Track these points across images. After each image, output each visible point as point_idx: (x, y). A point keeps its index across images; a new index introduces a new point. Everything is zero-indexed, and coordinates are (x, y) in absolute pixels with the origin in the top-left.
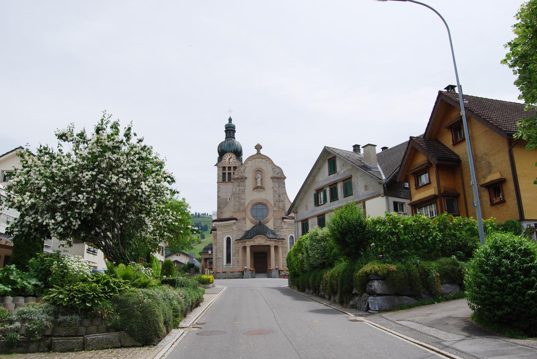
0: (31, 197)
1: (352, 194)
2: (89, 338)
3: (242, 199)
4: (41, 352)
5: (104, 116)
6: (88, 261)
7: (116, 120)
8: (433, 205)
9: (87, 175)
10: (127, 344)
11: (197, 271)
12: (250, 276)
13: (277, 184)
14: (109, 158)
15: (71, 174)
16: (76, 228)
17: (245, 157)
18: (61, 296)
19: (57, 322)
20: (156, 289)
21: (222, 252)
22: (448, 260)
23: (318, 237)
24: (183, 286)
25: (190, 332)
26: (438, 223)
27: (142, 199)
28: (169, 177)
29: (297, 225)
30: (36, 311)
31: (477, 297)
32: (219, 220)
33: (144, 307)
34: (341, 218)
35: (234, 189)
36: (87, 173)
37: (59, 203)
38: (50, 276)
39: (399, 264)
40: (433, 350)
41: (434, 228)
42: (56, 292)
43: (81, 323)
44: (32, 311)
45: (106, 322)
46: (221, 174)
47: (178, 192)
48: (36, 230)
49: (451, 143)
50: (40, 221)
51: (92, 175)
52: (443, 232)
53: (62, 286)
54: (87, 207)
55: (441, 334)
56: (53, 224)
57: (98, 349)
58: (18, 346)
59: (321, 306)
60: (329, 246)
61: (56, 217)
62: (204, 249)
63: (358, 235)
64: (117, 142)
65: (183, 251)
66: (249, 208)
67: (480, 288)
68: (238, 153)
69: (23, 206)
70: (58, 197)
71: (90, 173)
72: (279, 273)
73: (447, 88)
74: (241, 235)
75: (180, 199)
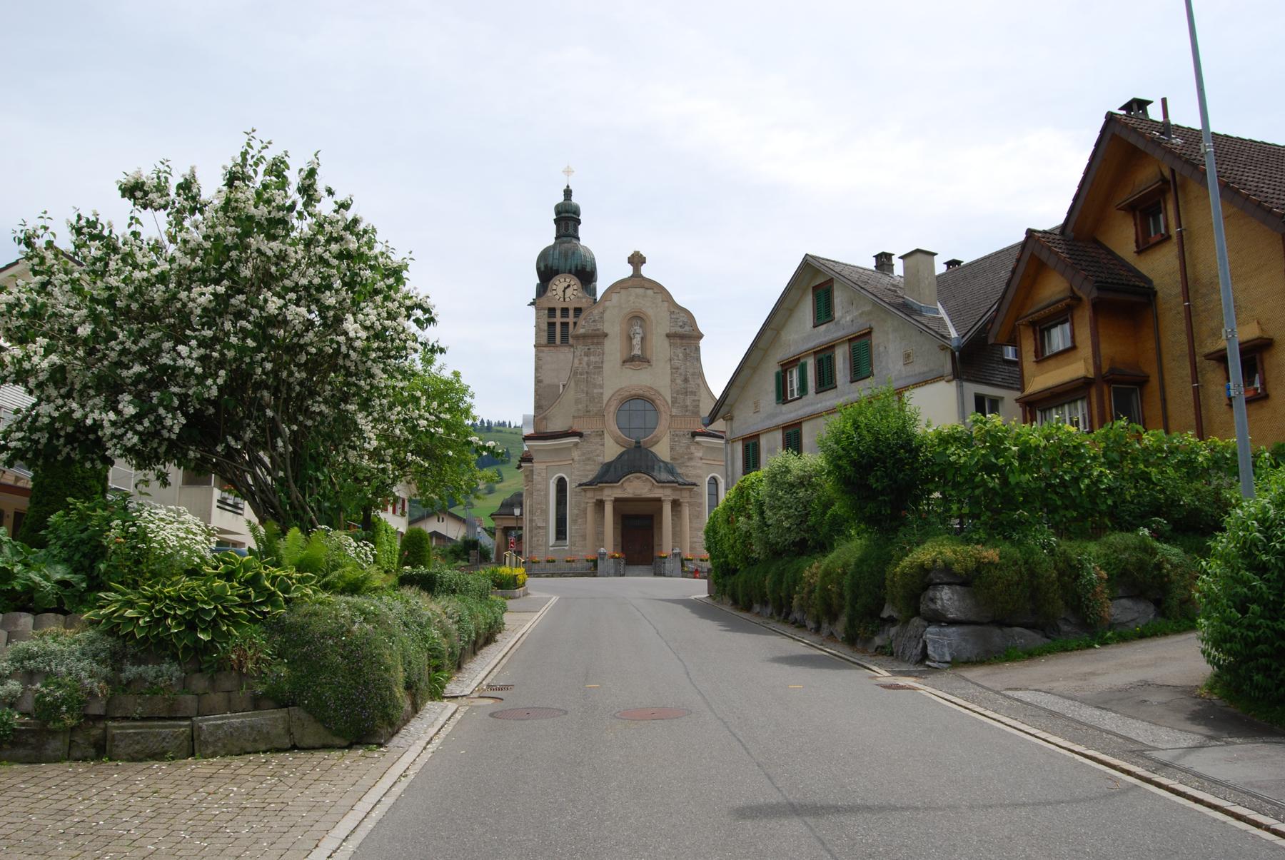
0: (48, 351)
1: (871, 374)
2: (207, 723)
3: (595, 386)
4: (77, 760)
5: (249, 145)
6: (193, 521)
7: (280, 153)
8: (1079, 403)
9: (203, 296)
10: (308, 741)
11: (484, 557)
12: (612, 571)
13: (680, 352)
14: (259, 250)
15: (158, 293)
16: (174, 437)
17: (602, 284)
18: (129, 613)
19: (120, 681)
20: (385, 599)
21: (546, 512)
22: (1129, 538)
23: (790, 478)
24: (454, 592)
25: (472, 709)
26: (1103, 445)
27: (348, 363)
28: (420, 306)
29: (733, 451)
30: (62, 652)
31: (1234, 636)
32: (539, 436)
33: (351, 643)
34: (856, 426)
35: (576, 361)
36: (204, 289)
37: (129, 368)
38: (103, 563)
39: (1006, 547)
40: (1129, 773)
41: (1094, 458)
42: (117, 601)
43: (185, 684)
44: (53, 652)
45: (251, 682)
46: (545, 327)
47: (442, 351)
48: (70, 439)
49: (1133, 247)
50: (78, 415)
51: (215, 294)
52: (1116, 468)
53: (135, 586)
54: (201, 379)
55: (1138, 730)
56: (113, 424)
57: (230, 753)
58: (14, 744)
59: (799, 648)
60: (819, 498)
61: (120, 406)
62: (502, 505)
63: (900, 471)
64: (280, 208)
65: (452, 510)
66: (612, 409)
67: (1243, 610)
68: (586, 275)
69: (27, 371)
70: (124, 352)
71: (211, 289)
72: (683, 565)
73: (1127, 107)
74: (591, 472)
75: (447, 374)
